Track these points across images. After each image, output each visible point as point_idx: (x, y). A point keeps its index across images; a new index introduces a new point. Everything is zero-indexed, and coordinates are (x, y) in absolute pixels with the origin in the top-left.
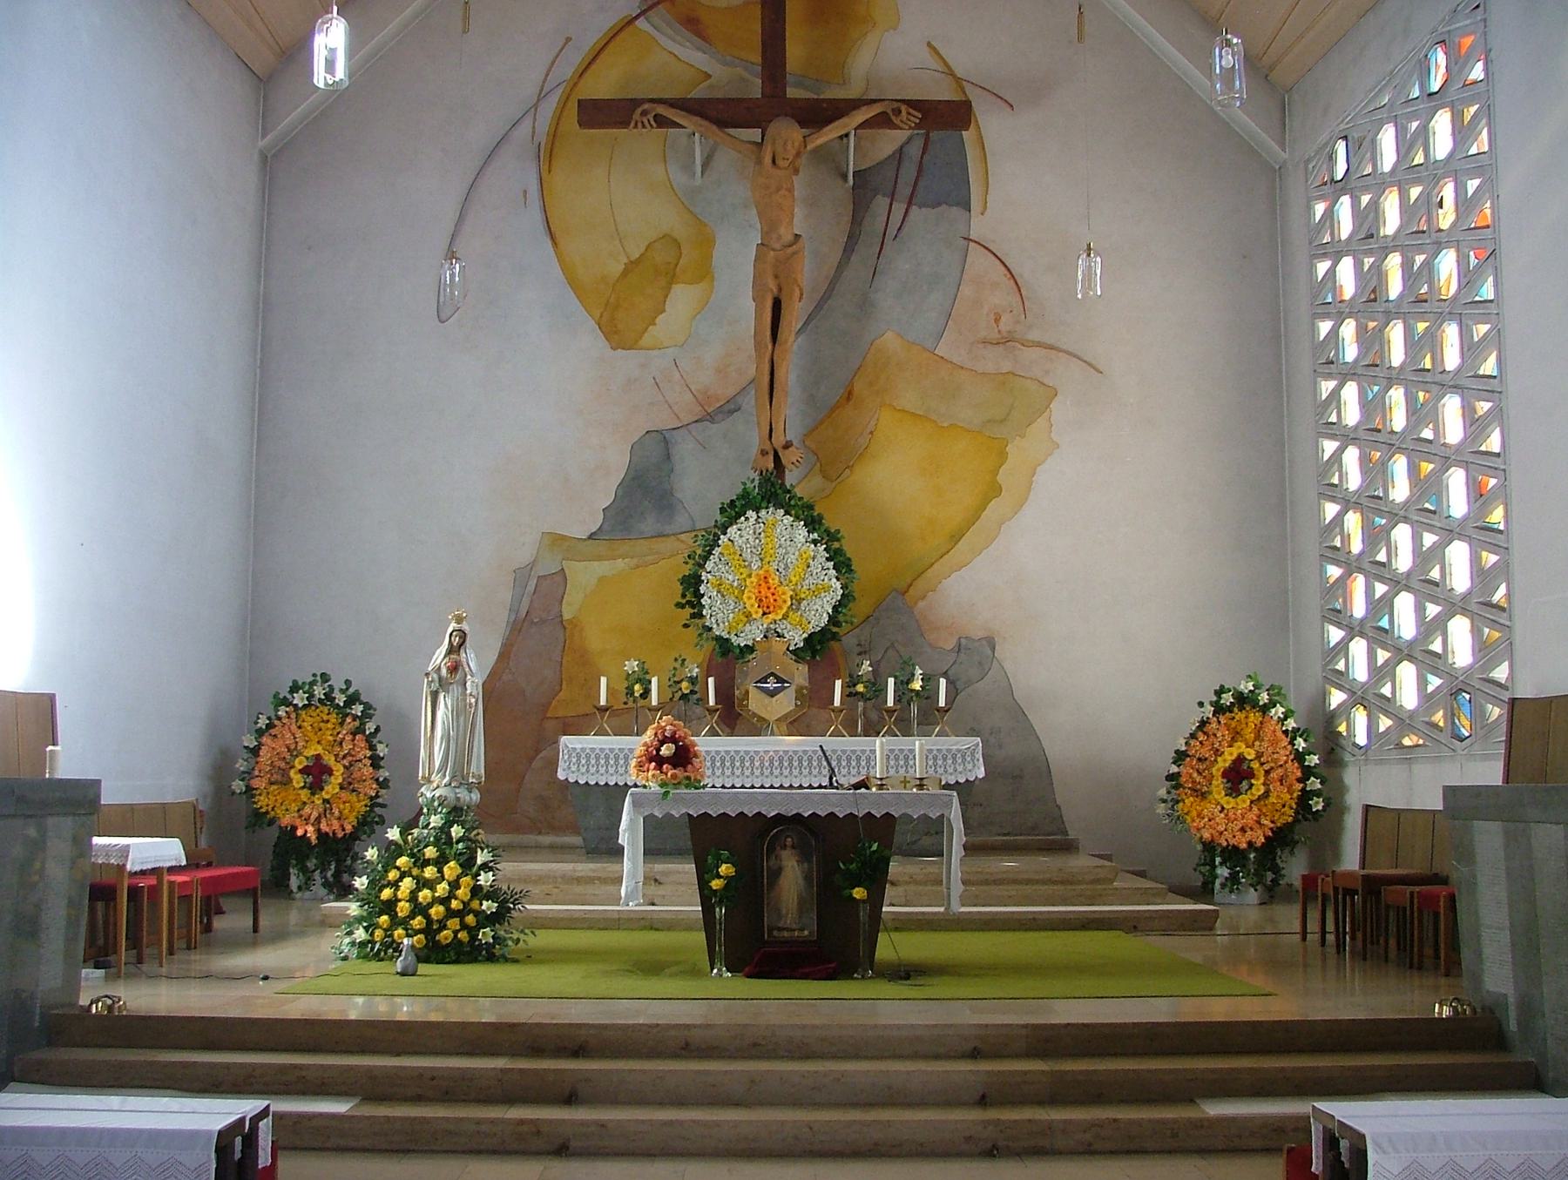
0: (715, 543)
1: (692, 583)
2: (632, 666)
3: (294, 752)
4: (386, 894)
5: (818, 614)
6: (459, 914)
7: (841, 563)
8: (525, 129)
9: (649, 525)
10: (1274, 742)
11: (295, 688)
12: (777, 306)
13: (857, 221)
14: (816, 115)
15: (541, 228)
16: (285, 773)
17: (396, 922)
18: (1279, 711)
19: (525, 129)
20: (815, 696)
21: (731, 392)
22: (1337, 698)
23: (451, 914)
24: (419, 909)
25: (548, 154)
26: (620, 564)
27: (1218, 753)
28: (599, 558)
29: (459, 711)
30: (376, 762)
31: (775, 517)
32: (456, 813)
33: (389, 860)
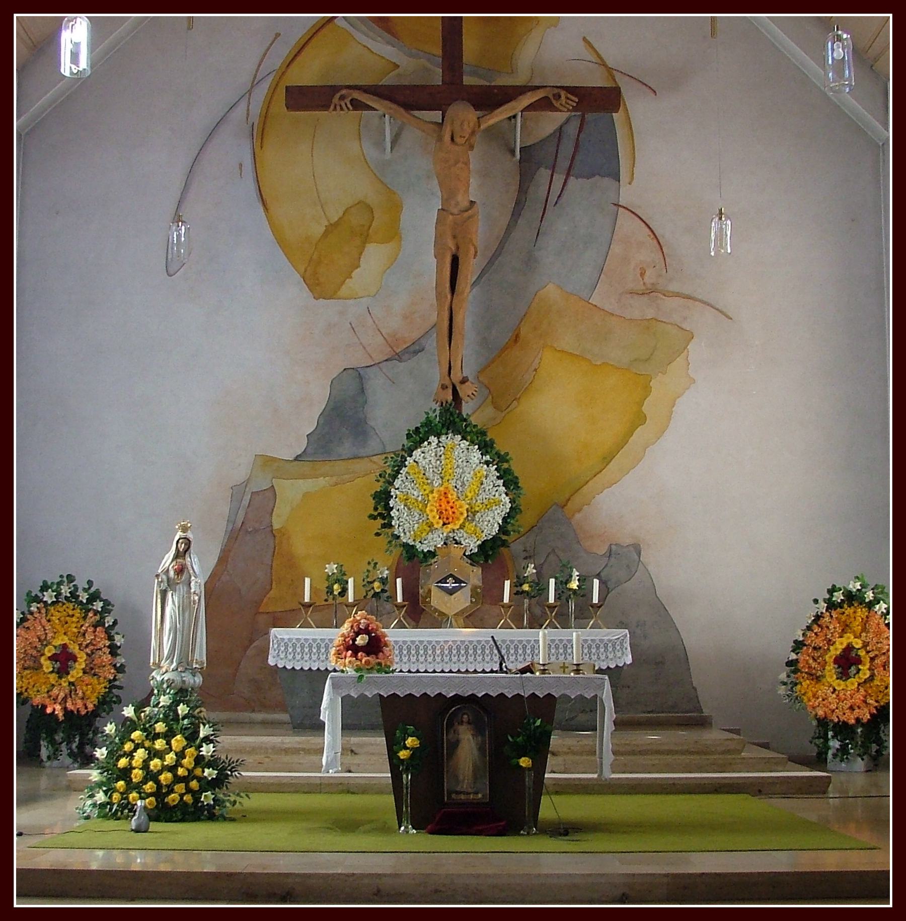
0: (402, 464)
1: (383, 498)
4: (123, 762)
6: (185, 780)
7: (510, 481)
8: (241, 110)
9: (346, 448)
11: (45, 587)
12: (455, 261)
13: (522, 191)
14: (488, 99)
15: (254, 195)
16: (36, 659)
19: (241, 110)
20: (488, 594)
21: (416, 335)
23: (177, 779)
24: (150, 775)
25: (260, 133)
26: (322, 482)
27: (830, 642)
28: (304, 477)
29: (185, 607)
30: (114, 650)
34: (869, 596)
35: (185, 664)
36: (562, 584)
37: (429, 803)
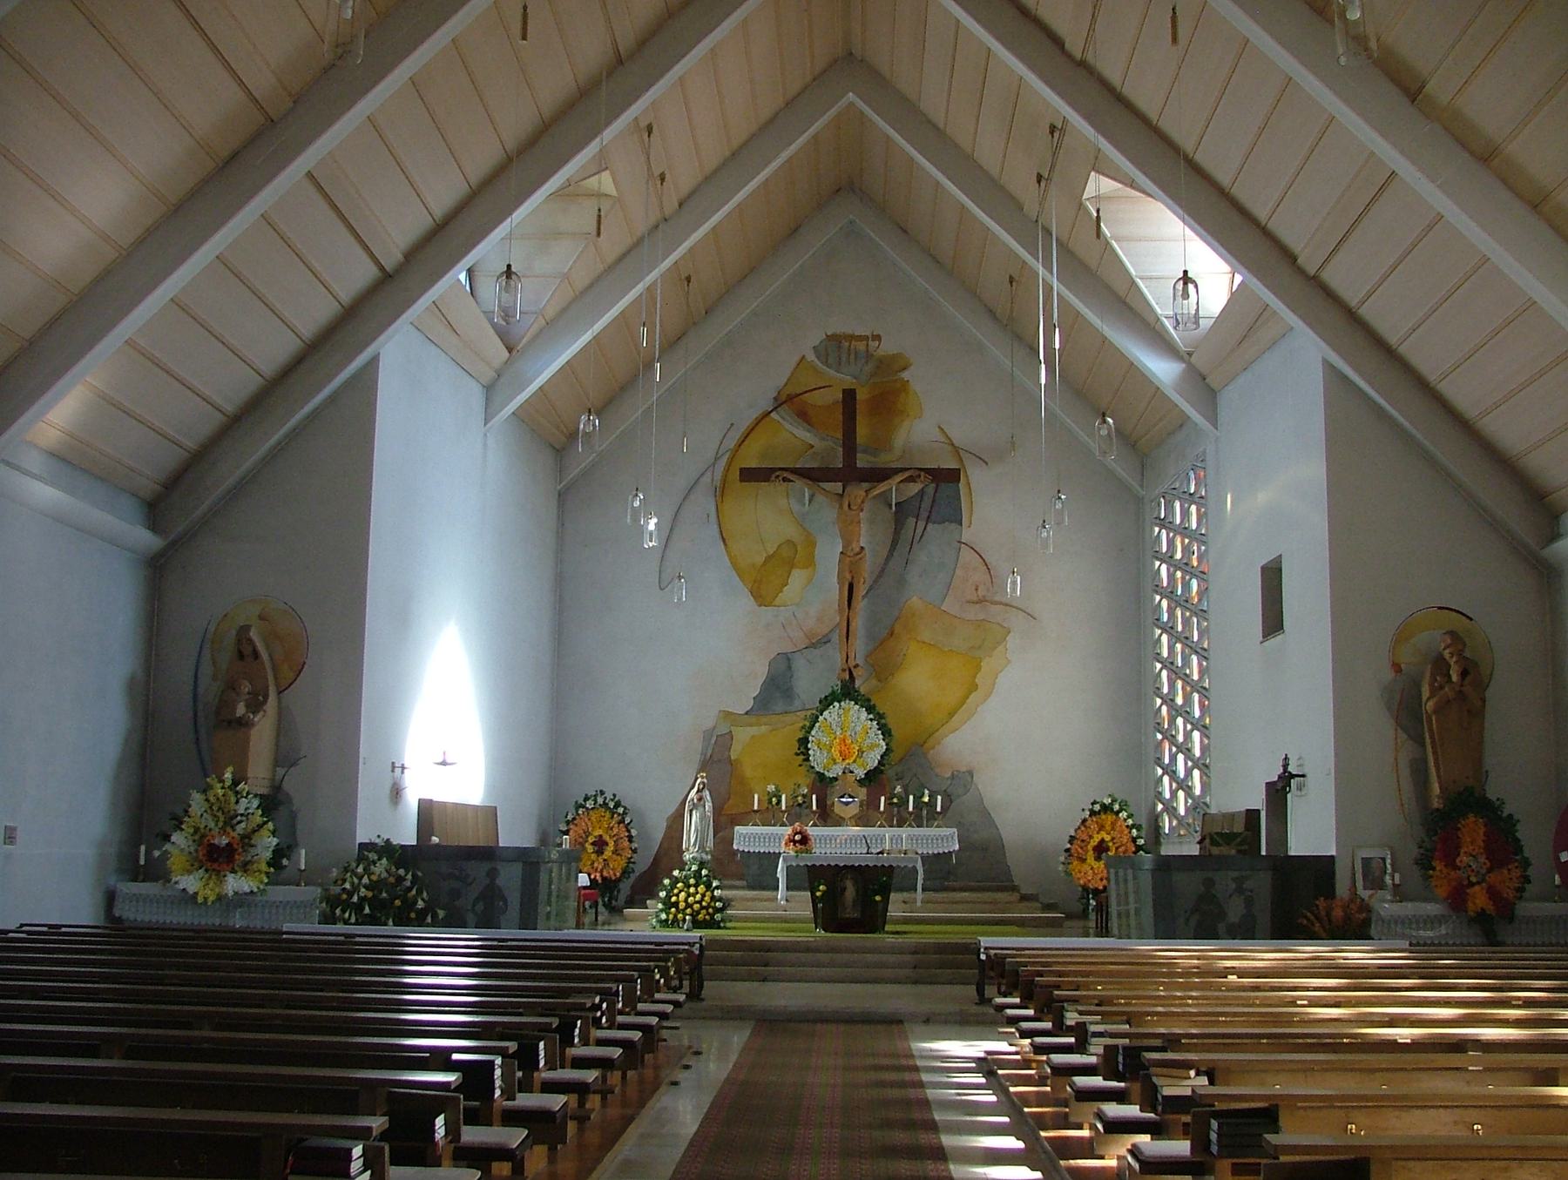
0: (816, 720)
1: (804, 742)
2: (771, 788)
3: (587, 834)
4: (674, 899)
5: (873, 760)
6: (706, 908)
7: (886, 731)
8: (707, 479)
9: (779, 707)
10: (1121, 832)
11: (586, 799)
13: (897, 532)
14: (878, 475)
15: (718, 536)
16: (582, 845)
17: (678, 911)
18: (1124, 815)
19: (707, 479)
20: (872, 803)
21: (826, 630)
22: (1160, 807)
23: (702, 908)
24: (688, 906)
25: (721, 492)
27: (1091, 837)
28: (751, 725)
29: (703, 818)
30: (630, 839)
31: (852, 708)
32: (702, 865)
33: (673, 885)
34: (1116, 807)
35: (702, 848)
36: (918, 799)
37: (829, 916)
